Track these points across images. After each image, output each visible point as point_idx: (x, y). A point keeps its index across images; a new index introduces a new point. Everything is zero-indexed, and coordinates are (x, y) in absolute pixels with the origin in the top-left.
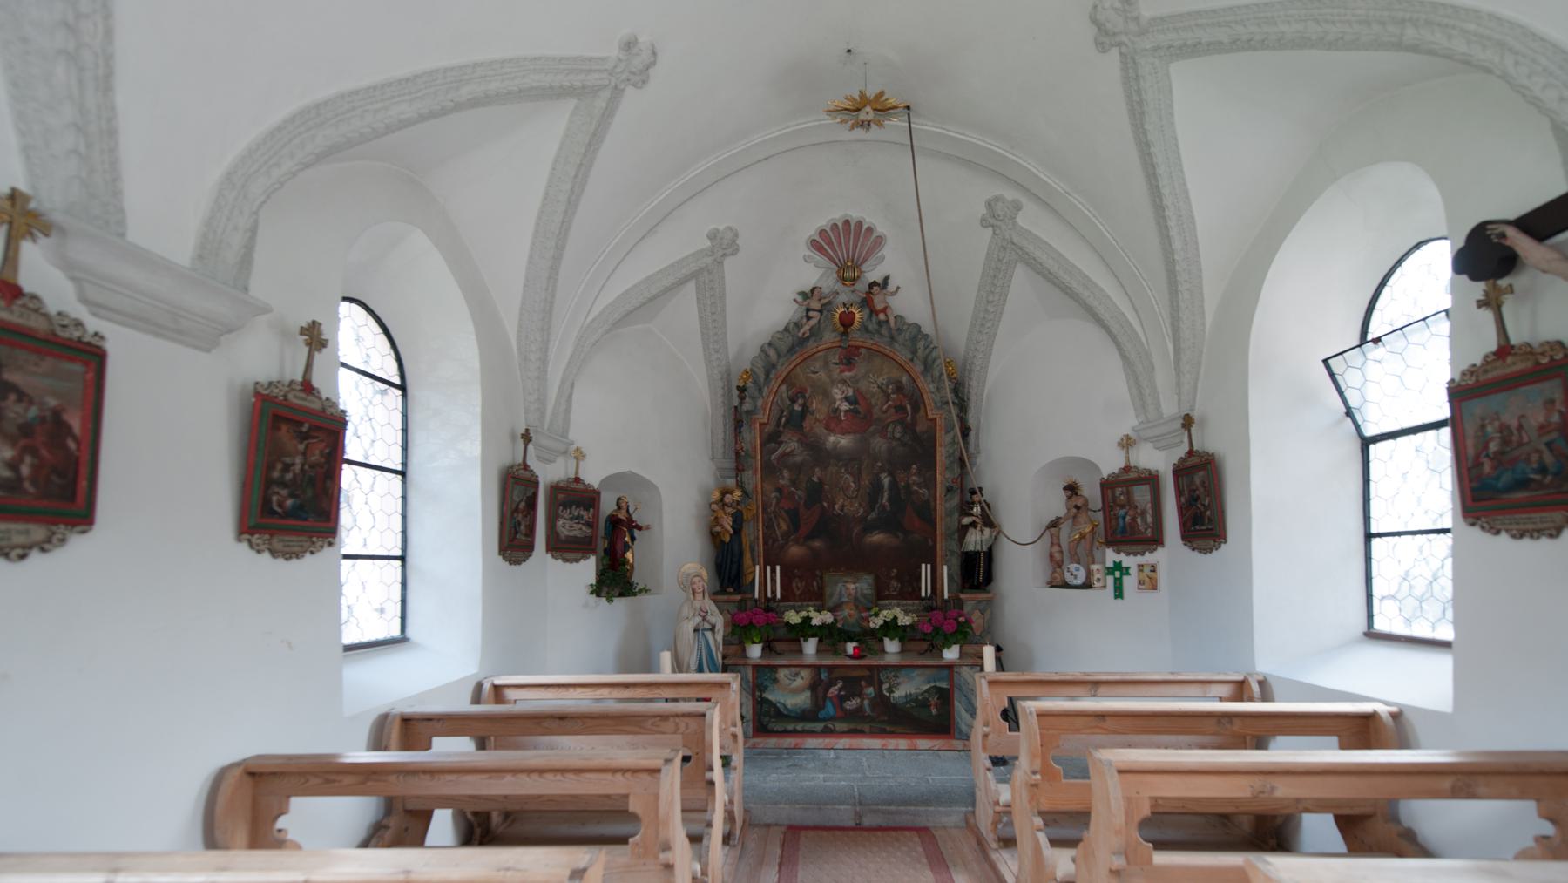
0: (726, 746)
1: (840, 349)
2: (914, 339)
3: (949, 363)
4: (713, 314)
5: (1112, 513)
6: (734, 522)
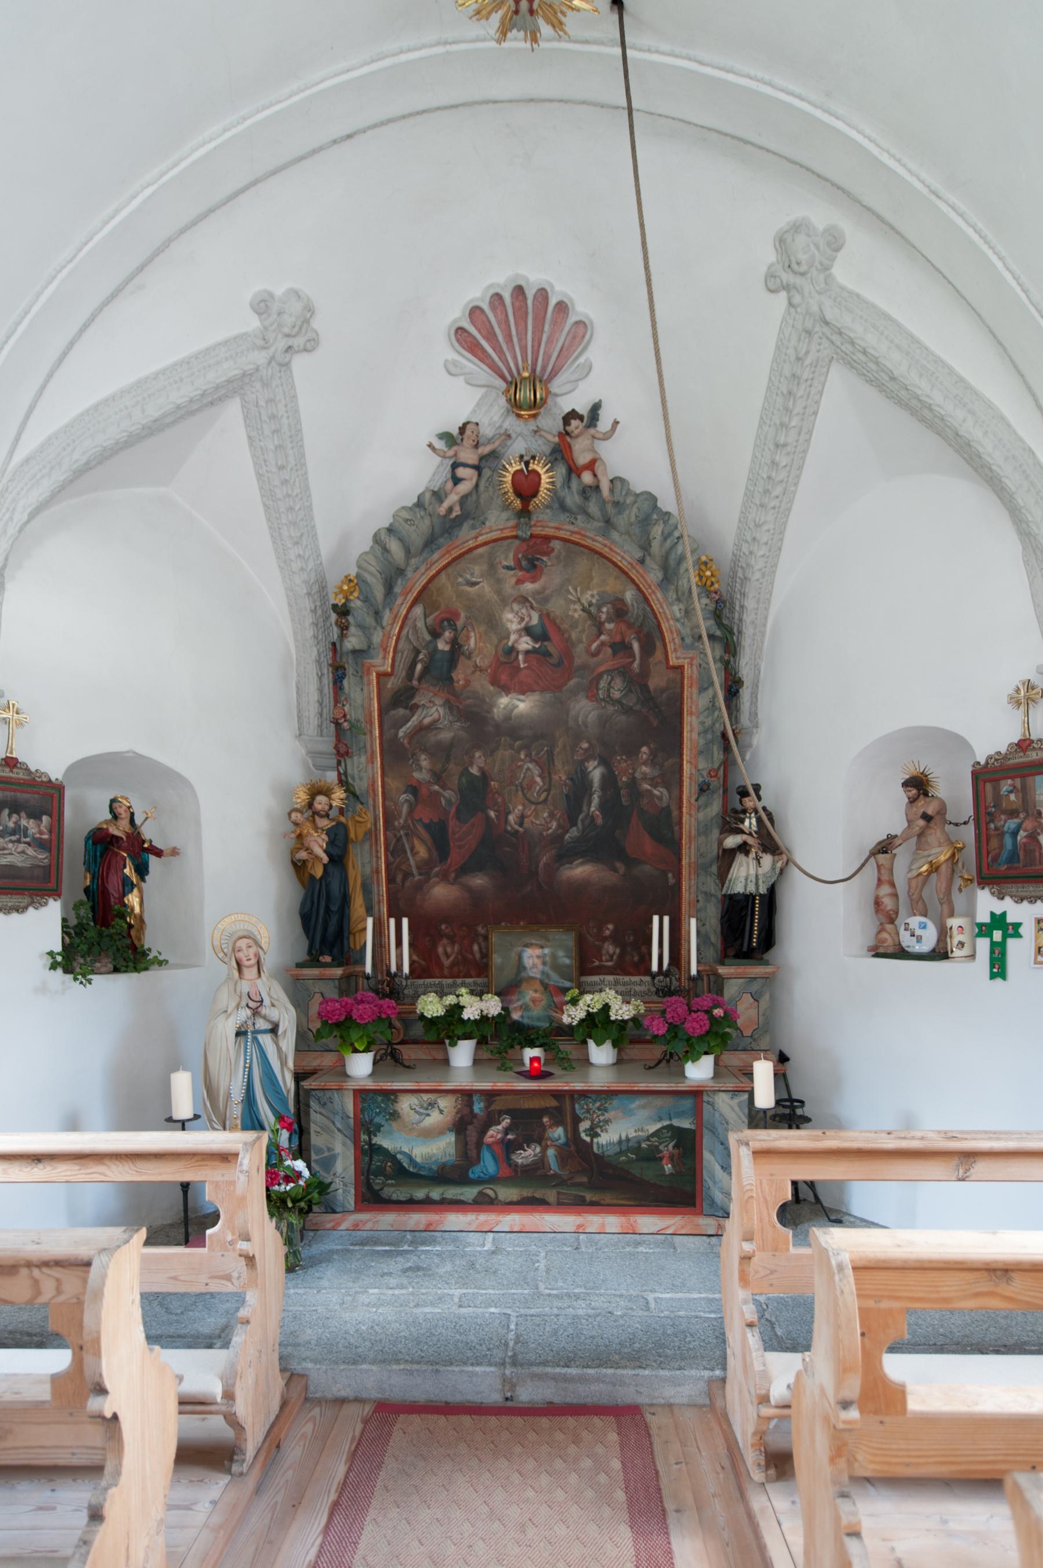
0: (235, 1275)
1: (517, 542)
2: (645, 522)
3: (705, 563)
4: (281, 468)
5: (992, 826)
6: (331, 843)
